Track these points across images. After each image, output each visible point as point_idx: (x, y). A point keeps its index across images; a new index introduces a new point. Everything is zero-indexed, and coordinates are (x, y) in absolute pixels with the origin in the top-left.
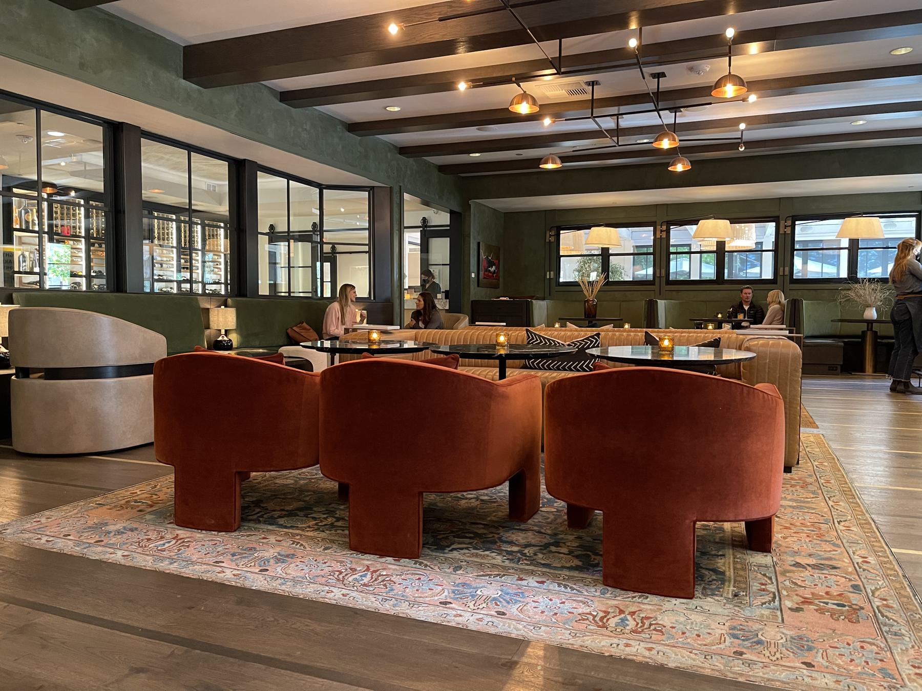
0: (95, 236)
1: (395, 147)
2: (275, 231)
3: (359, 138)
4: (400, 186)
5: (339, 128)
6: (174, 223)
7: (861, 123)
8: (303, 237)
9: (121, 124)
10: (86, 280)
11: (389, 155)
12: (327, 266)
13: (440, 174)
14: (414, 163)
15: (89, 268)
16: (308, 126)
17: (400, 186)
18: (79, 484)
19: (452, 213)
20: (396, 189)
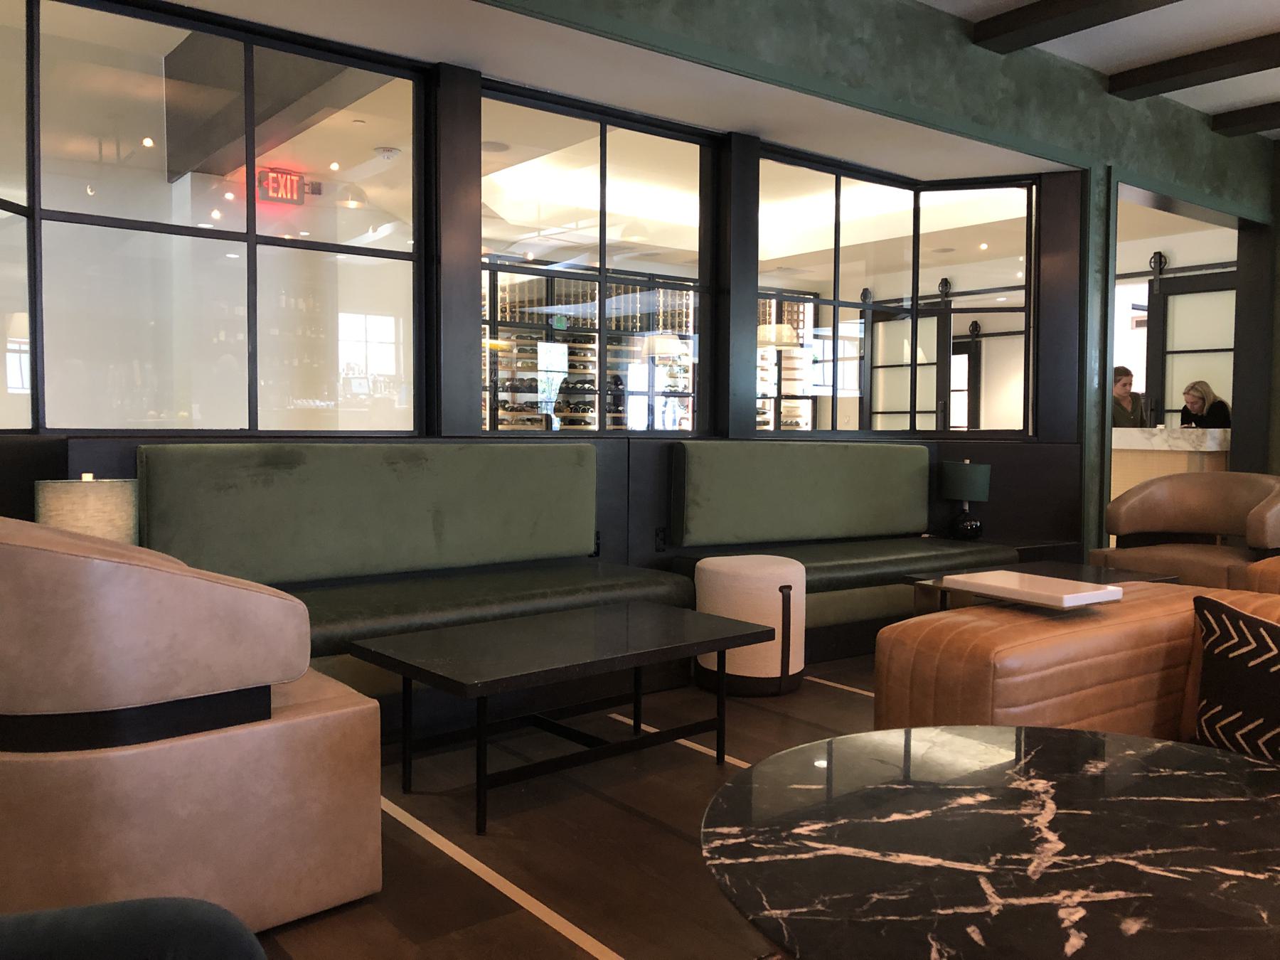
0: (508, 320)
1: (1096, 73)
2: (981, 333)
3: (1003, 57)
4: (1110, 168)
5: (950, 34)
6: (691, 293)
7: (877, 571)
8: (917, 310)
9: (438, 66)
10: (490, 394)
11: (1082, 95)
12: (959, 364)
13: (1216, 134)
14: (1148, 113)
15: (651, 384)
16: (866, 33)
17: (1110, 168)
18: (857, 591)
19: (1246, 228)
20: (1098, 174)
